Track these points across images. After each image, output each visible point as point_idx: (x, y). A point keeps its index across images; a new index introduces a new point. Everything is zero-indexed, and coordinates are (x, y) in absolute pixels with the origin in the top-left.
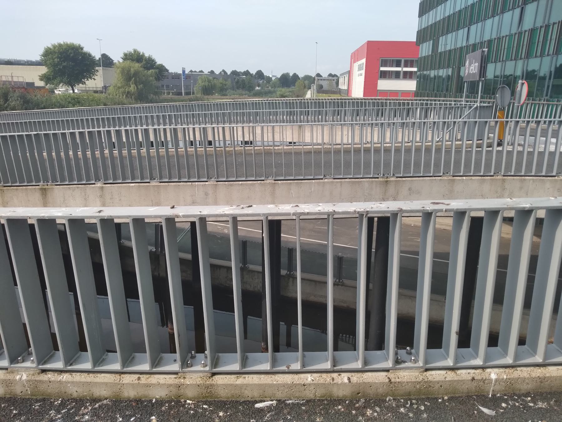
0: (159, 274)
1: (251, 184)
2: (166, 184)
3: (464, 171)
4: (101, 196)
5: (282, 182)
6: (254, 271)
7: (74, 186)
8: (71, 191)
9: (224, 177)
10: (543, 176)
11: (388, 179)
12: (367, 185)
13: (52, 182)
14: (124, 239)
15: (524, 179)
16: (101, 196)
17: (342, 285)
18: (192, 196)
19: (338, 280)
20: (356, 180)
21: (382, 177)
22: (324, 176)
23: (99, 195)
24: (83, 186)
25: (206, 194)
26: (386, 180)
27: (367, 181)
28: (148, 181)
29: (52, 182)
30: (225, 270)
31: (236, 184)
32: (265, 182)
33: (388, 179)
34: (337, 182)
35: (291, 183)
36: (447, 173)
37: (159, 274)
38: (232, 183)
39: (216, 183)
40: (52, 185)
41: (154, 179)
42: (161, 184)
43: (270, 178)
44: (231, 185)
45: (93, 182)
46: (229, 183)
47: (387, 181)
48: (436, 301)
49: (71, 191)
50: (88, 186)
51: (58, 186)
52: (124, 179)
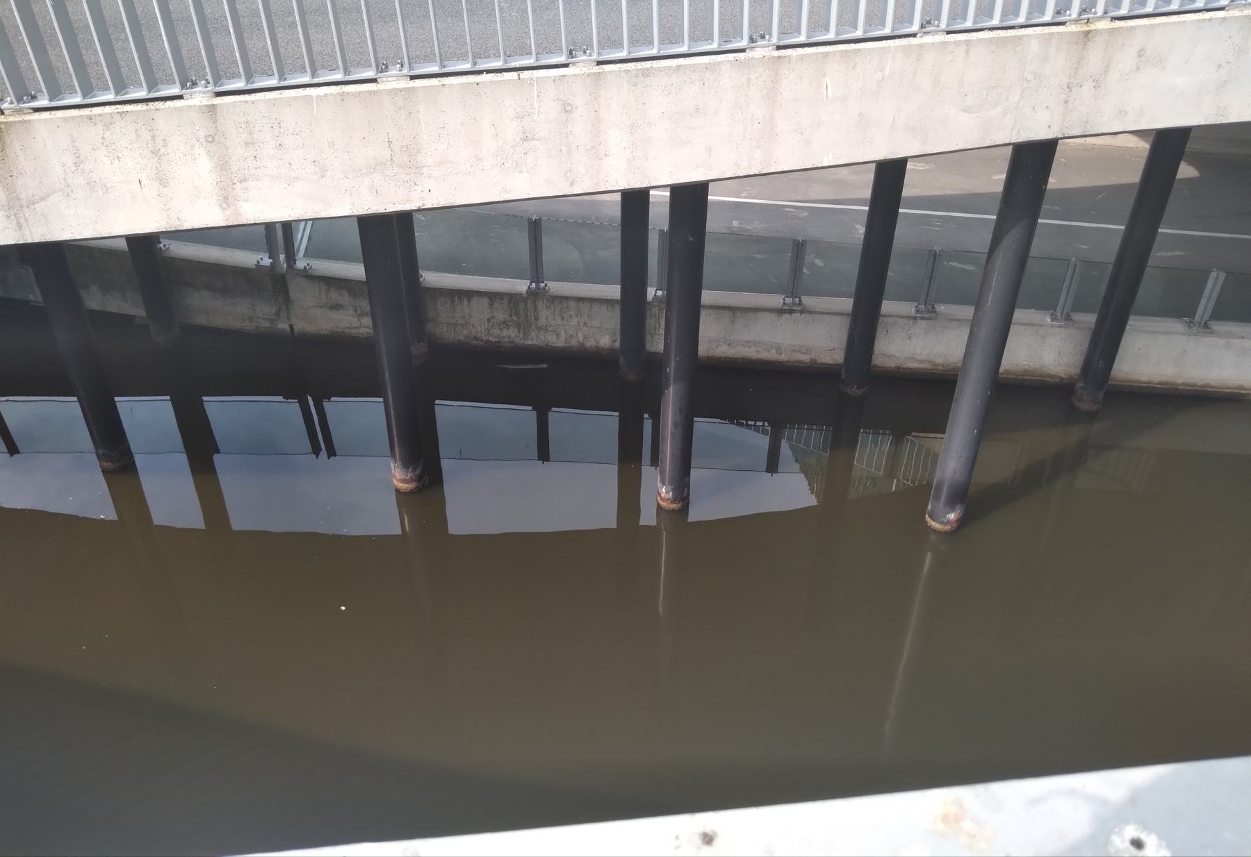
0: (291, 326)
1: (708, 67)
2: (434, 81)
3: (838, 24)
4: (211, 139)
5: (800, 51)
6: (567, 298)
7: (108, 109)
8: (100, 127)
9: (334, 69)
10: (1022, 27)
11: (1092, 27)
12: (1034, 46)
13: (20, 100)
14: (428, 269)
15: (1021, 37)
16: (211, 139)
17: (802, 312)
18: (520, 117)
19: (534, 285)
20: (1010, 33)
21: (1076, 21)
22: (752, 40)
23: (202, 134)
24: (140, 107)
25: (567, 108)
26: (1085, 28)
27: (1038, 36)
28: (370, 74)
29: (20, 100)
30: (486, 301)
31: (660, 69)
32: (749, 54)
33: (1092, 27)
34: (957, 43)
35: (826, 54)
36: (763, 37)
37: (291, 326)
38: (648, 64)
39: (598, 69)
40: (19, 111)
41: (194, 84)
42: (418, 83)
43: (394, 71)
44: (646, 73)
45: (175, 90)
46: (640, 65)
47: (1089, 32)
48: (1032, 325)
49: (100, 127)
50: (159, 105)
51: (45, 115)
52: (120, 87)
